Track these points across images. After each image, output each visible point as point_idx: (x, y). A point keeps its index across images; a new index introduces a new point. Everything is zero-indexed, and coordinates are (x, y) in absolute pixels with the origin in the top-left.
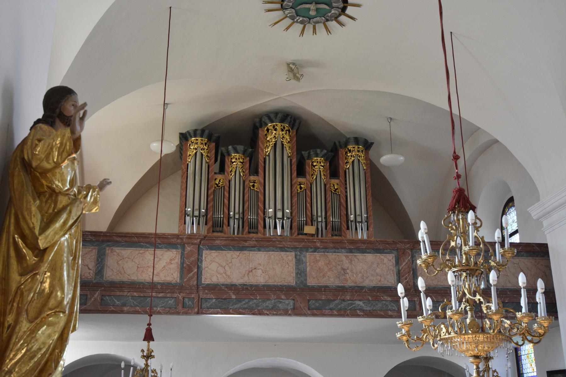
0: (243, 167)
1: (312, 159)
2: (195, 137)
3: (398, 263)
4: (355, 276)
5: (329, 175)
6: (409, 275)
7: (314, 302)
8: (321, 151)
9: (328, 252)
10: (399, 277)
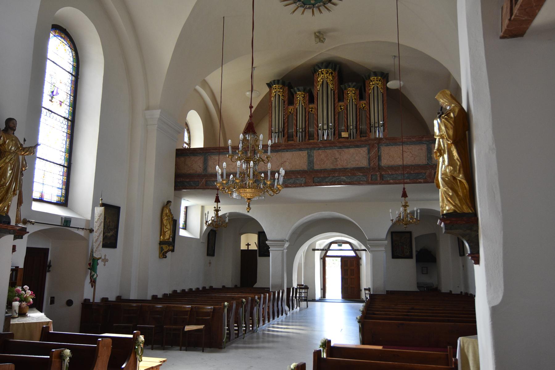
0: (304, 100)
1: (347, 89)
2: (278, 84)
3: (369, 152)
4: (342, 162)
5: (358, 98)
6: (375, 160)
7: (317, 178)
8: (352, 84)
9: (326, 149)
10: (370, 161)
